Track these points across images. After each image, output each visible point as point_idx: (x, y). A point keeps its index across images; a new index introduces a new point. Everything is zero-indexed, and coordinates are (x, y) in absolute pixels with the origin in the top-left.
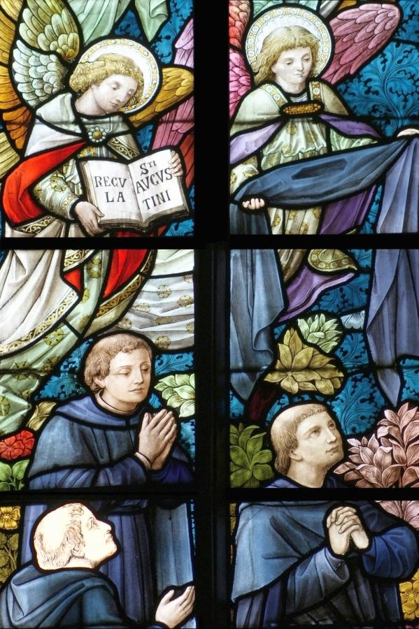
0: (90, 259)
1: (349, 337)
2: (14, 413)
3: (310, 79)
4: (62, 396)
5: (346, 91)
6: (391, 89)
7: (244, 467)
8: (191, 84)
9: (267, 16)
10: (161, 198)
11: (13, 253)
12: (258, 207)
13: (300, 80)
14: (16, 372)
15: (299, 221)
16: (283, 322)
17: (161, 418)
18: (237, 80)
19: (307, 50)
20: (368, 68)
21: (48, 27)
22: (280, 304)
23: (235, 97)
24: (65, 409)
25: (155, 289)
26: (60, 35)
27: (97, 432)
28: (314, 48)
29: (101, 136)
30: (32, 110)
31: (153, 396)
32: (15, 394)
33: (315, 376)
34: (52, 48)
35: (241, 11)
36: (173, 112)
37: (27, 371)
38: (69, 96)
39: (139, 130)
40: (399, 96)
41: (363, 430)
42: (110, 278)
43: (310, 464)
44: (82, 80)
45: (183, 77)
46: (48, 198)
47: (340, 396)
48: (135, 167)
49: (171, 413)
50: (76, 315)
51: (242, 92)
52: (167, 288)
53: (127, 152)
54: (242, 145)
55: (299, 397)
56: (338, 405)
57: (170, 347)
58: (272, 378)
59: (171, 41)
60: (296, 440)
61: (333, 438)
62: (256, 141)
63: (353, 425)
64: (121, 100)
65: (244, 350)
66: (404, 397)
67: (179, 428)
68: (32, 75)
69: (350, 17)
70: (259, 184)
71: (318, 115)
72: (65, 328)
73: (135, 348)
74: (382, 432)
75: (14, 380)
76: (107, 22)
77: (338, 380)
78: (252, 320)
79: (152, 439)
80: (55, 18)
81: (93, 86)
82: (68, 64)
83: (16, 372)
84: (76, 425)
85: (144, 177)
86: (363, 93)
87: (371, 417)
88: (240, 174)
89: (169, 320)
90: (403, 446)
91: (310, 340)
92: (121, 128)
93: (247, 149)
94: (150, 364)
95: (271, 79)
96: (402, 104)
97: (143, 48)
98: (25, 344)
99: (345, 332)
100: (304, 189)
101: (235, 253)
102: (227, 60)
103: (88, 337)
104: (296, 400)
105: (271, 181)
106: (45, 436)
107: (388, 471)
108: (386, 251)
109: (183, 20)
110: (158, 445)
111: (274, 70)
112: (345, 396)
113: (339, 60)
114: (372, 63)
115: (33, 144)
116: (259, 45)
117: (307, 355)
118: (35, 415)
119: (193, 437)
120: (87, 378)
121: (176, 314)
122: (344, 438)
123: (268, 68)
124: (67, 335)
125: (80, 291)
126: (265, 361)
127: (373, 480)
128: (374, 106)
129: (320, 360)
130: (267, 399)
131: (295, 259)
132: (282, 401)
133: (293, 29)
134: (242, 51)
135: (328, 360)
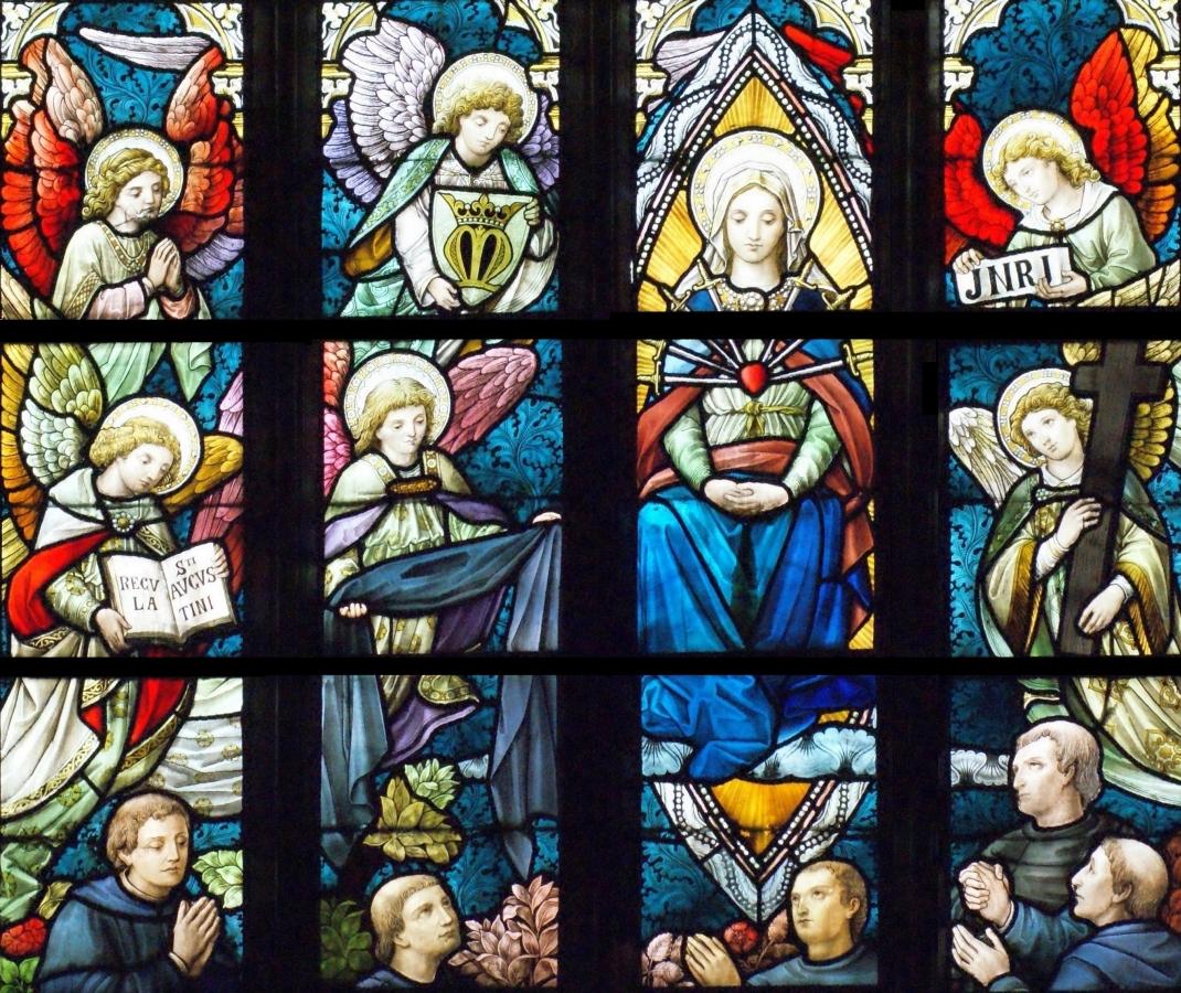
0: (114, 693)
1: (468, 789)
2: (21, 895)
3: (424, 446)
4: (80, 875)
5: (469, 463)
6: (525, 461)
7: (337, 953)
8: (239, 457)
9: (371, 365)
10: (201, 606)
11: (21, 682)
12: (358, 614)
13: (411, 448)
14: (23, 840)
15: (410, 632)
16: (386, 767)
17: (201, 908)
18: (334, 449)
19: (420, 410)
20: (496, 432)
21: (64, 382)
22: (383, 745)
23: (331, 472)
24: (84, 892)
25: (193, 734)
26: (79, 391)
27: (123, 923)
28: (429, 407)
29: (128, 524)
30: (45, 489)
31: (191, 879)
32: (23, 869)
33: (426, 839)
34: (69, 409)
35: (339, 359)
36: (217, 494)
37: (34, 839)
38: (89, 471)
39: (176, 517)
40: (535, 469)
41: (485, 909)
42: (139, 719)
43: (420, 952)
44: (104, 451)
45: (229, 448)
46: (63, 603)
47: (457, 865)
48: (170, 564)
49: (212, 901)
50: (97, 766)
51: (339, 464)
52: (209, 734)
53: (160, 545)
54: (341, 533)
55: (407, 866)
56: (455, 877)
57: (213, 814)
58: (373, 840)
59: (214, 401)
60: (402, 921)
61: (448, 920)
62: (357, 529)
63: (474, 903)
64: (153, 478)
65: (338, 803)
66: (537, 867)
67: (223, 923)
68: (45, 443)
69: (473, 366)
70: (360, 585)
71: (433, 495)
72: (83, 784)
73: (169, 814)
74: (509, 912)
75: (22, 850)
76: (136, 377)
77: (454, 847)
78: (348, 766)
79: (189, 935)
80: (73, 370)
81: (119, 459)
82: (88, 430)
83: (23, 840)
84: (96, 915)
85: (180, 578)
86: (490, 466)
87: (494, 894)
88: (337, 571)
89: (212, 777)
90: (535, 930)
91: (419, 793)
92: (152, 515)
93: (345, 540)
94: (187, 835)
95: (375, 447)
96: (538, 480)
97: (182, 411)
98: (35, 803)
99: (463, 782)
100: (418, 591)
101: (327, 679)
102: (322, 423)
103: (112, 796)
104: (403, 869)
105: (376, 581)
106: (58, 926)
107: (515, 963)
108: (516, 677)
109: (229, 373)
110: (197, 944)
111: (379, 436)
112: (463, 865)
113: (460, 422)
114: (502, 425)
115: (46, 533)
116: (361, 404)
117: (416, 812)
118: (46, 899)
119: (241, 936)
120: (110, 852)
121: (220, 769)
122: (462, 919)
123: (371, 434)
124: (85, 793)
125: (102, 735)
126: (364, 819)
127: (497, 974)
128: (503, 483)
129: (432, 818)
130: (367, 868)
131: (402, 687)
132: (384, 870)
133: (402, 382)
134: (339, 411)
135: (442, 818)
